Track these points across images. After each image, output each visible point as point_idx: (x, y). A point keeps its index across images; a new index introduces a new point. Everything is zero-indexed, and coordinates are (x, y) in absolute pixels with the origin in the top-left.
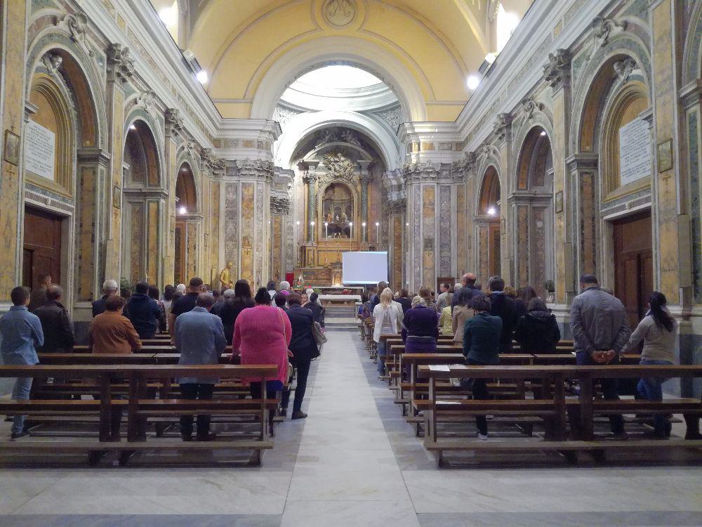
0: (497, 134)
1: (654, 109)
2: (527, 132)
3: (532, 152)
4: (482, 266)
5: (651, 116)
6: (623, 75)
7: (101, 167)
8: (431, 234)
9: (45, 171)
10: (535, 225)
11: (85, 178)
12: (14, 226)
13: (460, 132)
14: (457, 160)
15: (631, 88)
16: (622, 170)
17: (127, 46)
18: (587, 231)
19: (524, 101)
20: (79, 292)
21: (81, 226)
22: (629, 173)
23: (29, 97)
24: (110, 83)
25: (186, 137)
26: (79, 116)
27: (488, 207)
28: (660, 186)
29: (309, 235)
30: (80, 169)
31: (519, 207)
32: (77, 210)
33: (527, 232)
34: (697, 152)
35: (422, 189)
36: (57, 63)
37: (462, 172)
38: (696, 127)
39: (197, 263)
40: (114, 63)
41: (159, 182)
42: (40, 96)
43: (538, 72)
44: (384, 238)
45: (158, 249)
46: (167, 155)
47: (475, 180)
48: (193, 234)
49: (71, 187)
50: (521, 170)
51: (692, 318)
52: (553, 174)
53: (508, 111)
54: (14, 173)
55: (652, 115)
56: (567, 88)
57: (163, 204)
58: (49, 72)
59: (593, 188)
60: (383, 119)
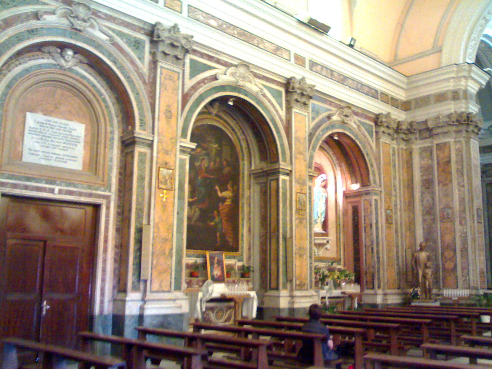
40: (157, 42)
48: (369, 211)
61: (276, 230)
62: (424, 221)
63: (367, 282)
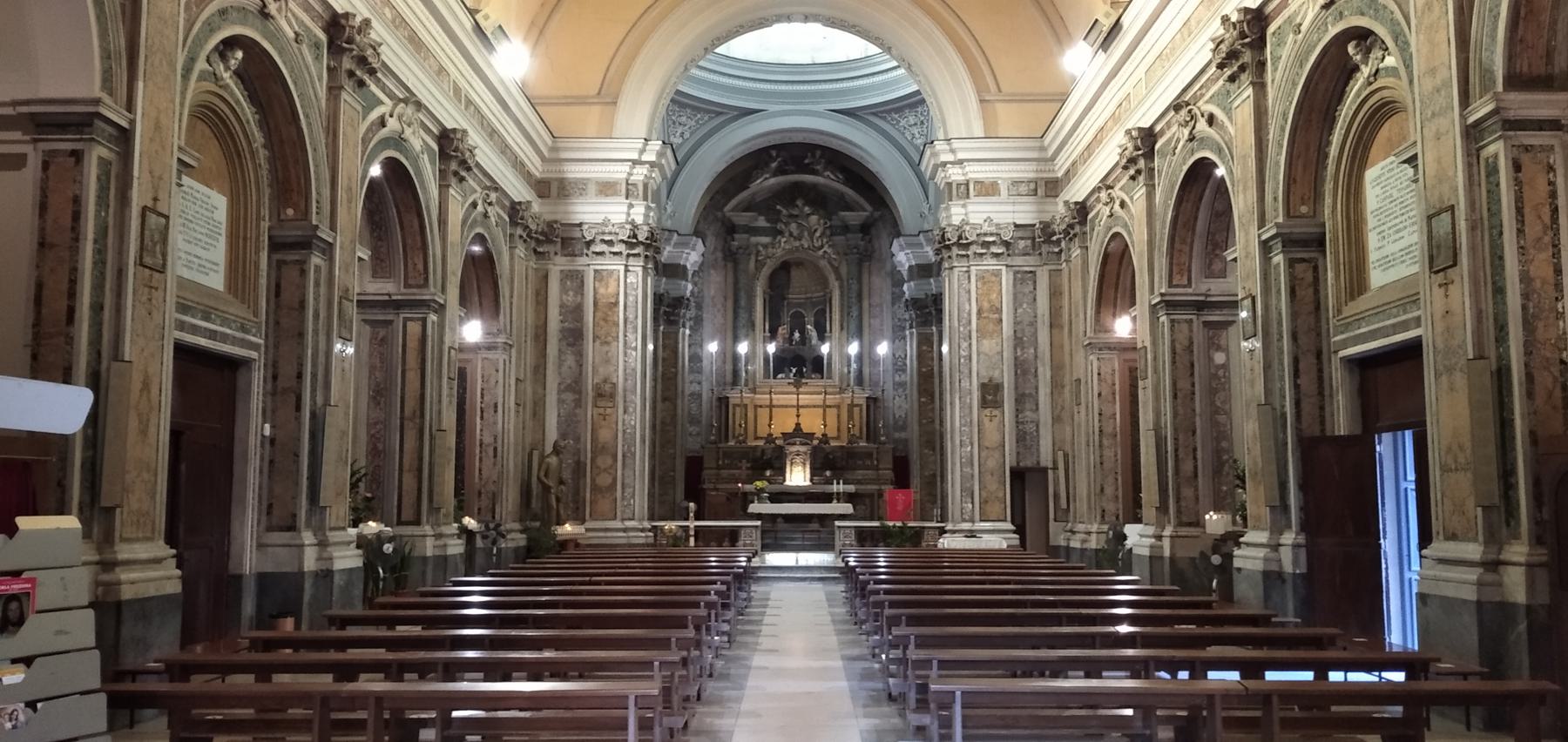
0: (1125, 168)
1: (1419, 144)
2: (1185, 168)
3: (1198, 209)
4: (1105, 442)
5: (1415, 157)
6: (1367, 65)
7: (316, 260)
8: (996, 374)
9: (207, 274)
10: (1210, 359)
11: (283, 284)
12: (154, 391)
13: (1053, 159)
14: (1047, 218)
15: (1385, 93)
16: (1373, 256)
17: (367, 14)
18: (1307, 381)
19: (1176, 106)
20: (269, 513)
21: (275, 378)
22: (1387, 262)
23: (183, 137)
24: (334, 90)
25: (480, 183)
26: (272, 160)
27: (1114, 316)
28: (1434, 300)
29: (736, 373)
30: (274, 264)
31: (1172, 321)
32: (266, 347)
33: (1192, 374)
34: (1501, 233)
35: (973, 279)
36: (233, 62)
37: (1059, 241)
38: (1498, 185)
39: (500, 442)
41: (426, 279)
42: (201, 126)
43: (1199, 54)
44: (897, 378)
45: (422, 415)
46: (443, 222)
47: (1086, 259)
48: (493, 381)
49: (256, 303)
50: (1177, 246)
51: (1502, 568)
52: (1235, 260)
53: (1146, 124)
54: (156, 289)
55: (1416, 154)
56: (1260, 87)
57: (433, 323)
58: (216, 78)
59: (1317, 292)
60: (893, 125)
61: (418, 413)
62: (560, 401)
63: (479, 509)
